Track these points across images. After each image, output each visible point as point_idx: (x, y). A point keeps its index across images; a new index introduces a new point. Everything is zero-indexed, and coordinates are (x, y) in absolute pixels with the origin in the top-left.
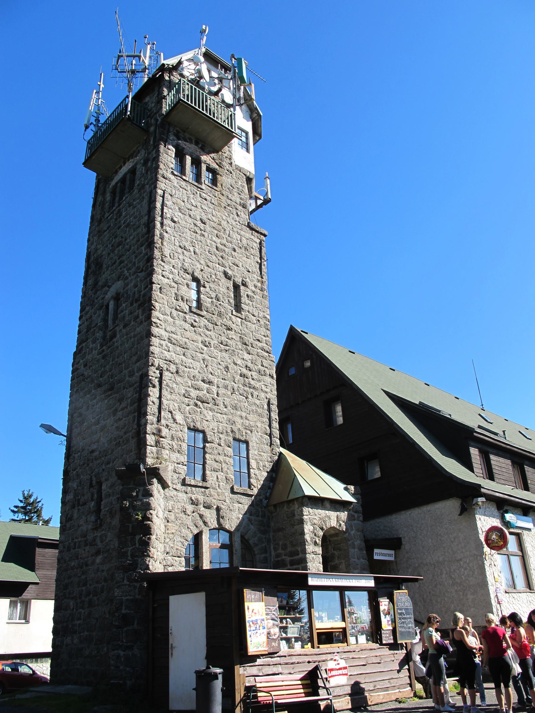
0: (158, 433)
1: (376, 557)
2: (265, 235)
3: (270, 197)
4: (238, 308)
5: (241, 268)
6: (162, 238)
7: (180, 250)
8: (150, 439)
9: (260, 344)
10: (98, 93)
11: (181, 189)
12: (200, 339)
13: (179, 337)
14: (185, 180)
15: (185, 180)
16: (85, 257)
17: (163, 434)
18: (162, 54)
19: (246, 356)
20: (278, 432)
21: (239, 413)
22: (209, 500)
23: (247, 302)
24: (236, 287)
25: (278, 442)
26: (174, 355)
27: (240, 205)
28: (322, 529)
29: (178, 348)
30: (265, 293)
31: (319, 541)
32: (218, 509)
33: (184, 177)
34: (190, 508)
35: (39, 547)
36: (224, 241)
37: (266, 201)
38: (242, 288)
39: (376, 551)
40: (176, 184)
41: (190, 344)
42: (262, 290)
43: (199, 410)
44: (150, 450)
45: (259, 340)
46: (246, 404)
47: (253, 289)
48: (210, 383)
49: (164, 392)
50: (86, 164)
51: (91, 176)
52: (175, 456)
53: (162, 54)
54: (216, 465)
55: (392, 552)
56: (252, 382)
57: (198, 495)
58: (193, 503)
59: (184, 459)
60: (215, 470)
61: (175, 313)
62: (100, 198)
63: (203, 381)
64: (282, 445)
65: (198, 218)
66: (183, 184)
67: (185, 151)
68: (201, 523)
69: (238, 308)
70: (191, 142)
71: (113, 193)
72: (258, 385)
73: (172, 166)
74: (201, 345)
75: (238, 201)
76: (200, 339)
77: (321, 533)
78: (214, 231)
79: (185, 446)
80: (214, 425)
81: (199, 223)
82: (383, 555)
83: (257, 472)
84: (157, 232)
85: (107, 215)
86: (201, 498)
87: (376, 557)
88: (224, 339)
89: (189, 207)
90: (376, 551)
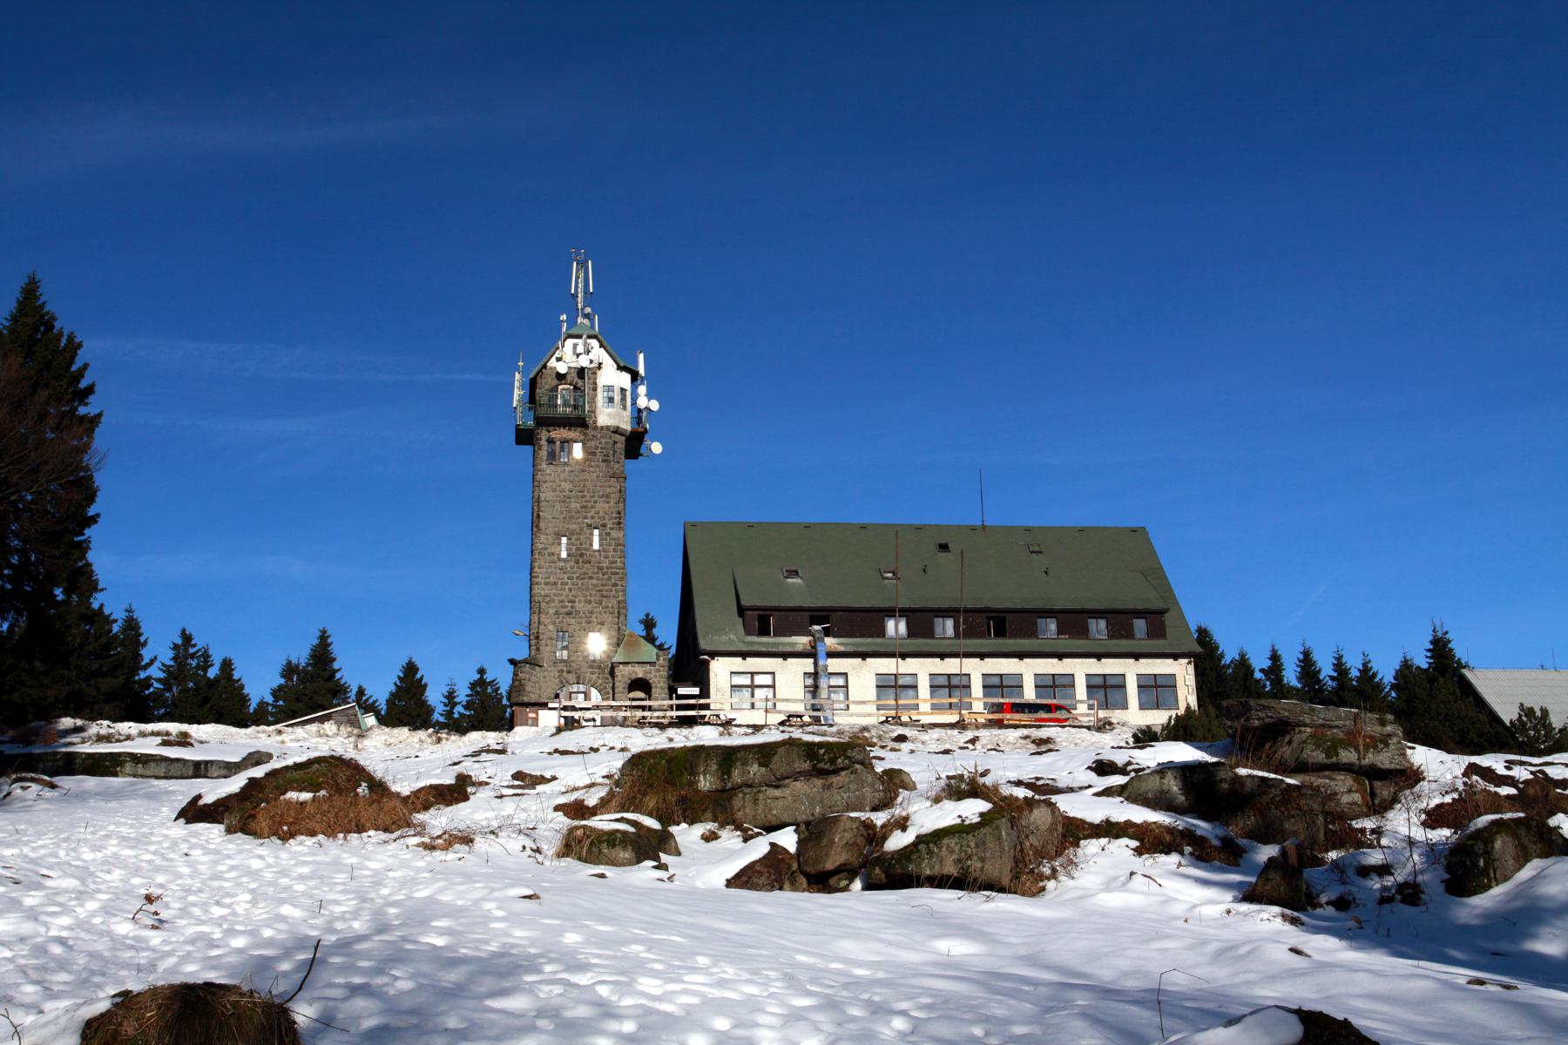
1: (698, 689)
13: (552, 580)
29: (550, 587)
74: (566, 580)
77: (629, 681)
87: (698, 689)
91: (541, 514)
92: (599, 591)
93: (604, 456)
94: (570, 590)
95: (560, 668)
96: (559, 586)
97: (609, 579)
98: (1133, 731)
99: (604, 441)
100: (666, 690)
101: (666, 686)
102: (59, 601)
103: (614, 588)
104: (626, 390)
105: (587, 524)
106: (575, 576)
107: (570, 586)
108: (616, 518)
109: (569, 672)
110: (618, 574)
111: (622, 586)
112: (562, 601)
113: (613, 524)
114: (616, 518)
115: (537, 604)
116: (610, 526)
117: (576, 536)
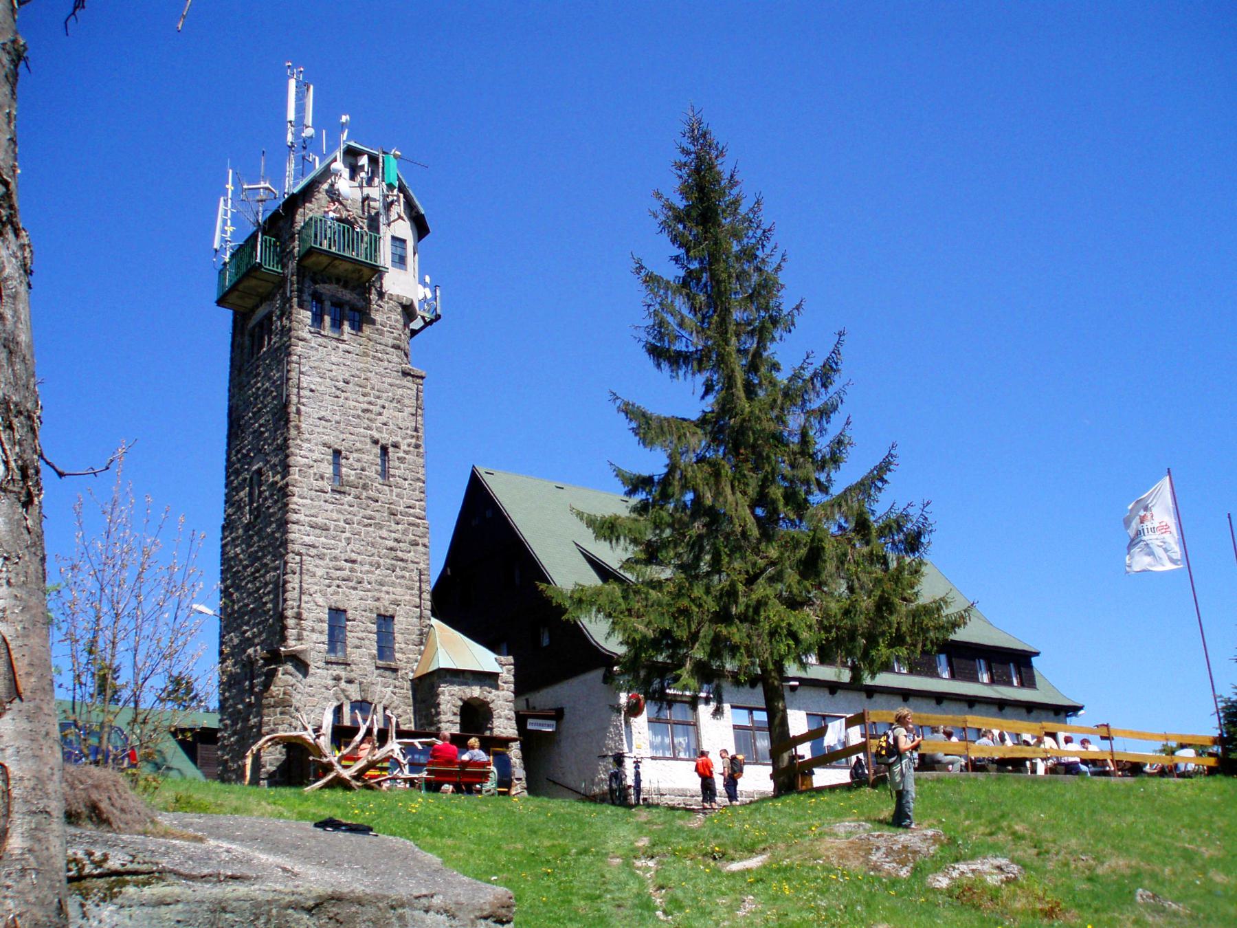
0: (299, 616)
1: (529, 727)
2: (422, 378)
3: (439, 312)
4: (385, 473)
5: (392, 427)
6: (298, 412)
7: (318, 422)
8: (291, 622)
9: (411, 511)
10: (226, 202)
11: (320, 348)
12: (342, 517)
13: (320, 520)
14: (323, 336)
15: (323, 336)
16: (226, 411)
17: (304, 616)
18: (312, 87)
19: (394, 526)
20: (429, 603)
21: (384, 589)
22: (353, 675)
23: (397, 464)
24: (384, 450)
25: (429, 613)
26: (313, 538)
27: (392, 347)
28: (461, 699)
29: (318, 531)
30: (421, 450)
31: (456, 710)
32: (361, 683)
33: (323, 333)
34: (331, 683)
35: (202, 743)
36: (372, 399)
37: (438, 317)
38: (391, 449)
39: (530, 721)
40: (313, 344)
41: (332, 525)
42: (417, 446)
43: (340, 590)
44: (291, 633)
45: (410, 507)
46: (394, 578)
47: (406, 448)
48: (354, 562)
49: (305, 577)
50: (221, 302)
51: (227, 315)
52: (315, 636)
53: (312, 87)
54: (357, 642)
55: (554, 722)
56: (400, 554)
57: (338, 671)
58: (337, 679)
59: (325, 638)
60: (357, 647)
61: (313, 493)
62: (237, 339)
63: (346, 561)
64: (434, 614)
65: (341, 378)
66: (320, 340)
67: (324, 297)
68: (342, 696)
69: (385, 473)
70: (331, 283)
71: (252, 335)
72: (410, 556)
73: (309, 322)
74: (342, 524)
75: (391, 342)
76: (342, 517)
77: (460, 703)
78: (357, 389)
79: (325, 626)
80: (355, 603)
81: (341, 384)
82: (536, 724)
83: (403, 646)
84: (293, 409)
85: (246, 366)
86: (343, 674)
87: (529, 727)
88: (369, 512)
89: (329, 366)
90: (530, 721)
91: (302, 408)
92: (391, 549)
93: (395, 339)
94: (348, 540)
95: (335, 673)
96: (332, 532)
97: (405, 532)
98: (915, 512)
99: (1167, 871)
100: (513, 722)
101: (512, 714)
102: (547, 646)
103: (412, 548)
104: (404, 241)
105: (372, 437)
106: (355, 519)
107: (347, 535)
108: (413, 437)
109: (350, 681)
110: (418, 526)
111: (424, 545)
112: (336, 558)
113: (409, 445)
114: (413, 437)
115: (298, 558)
116: (404, 447)
117: (355, 455)
